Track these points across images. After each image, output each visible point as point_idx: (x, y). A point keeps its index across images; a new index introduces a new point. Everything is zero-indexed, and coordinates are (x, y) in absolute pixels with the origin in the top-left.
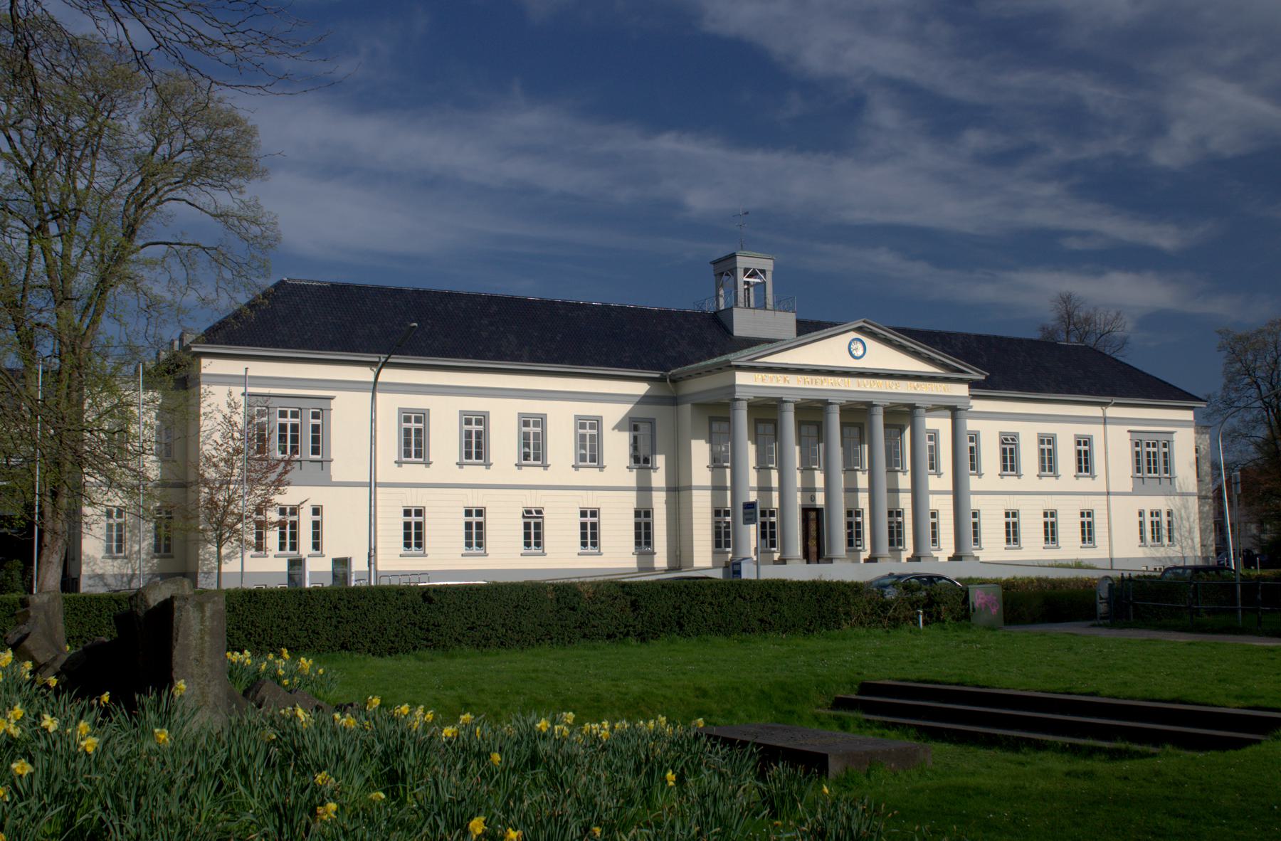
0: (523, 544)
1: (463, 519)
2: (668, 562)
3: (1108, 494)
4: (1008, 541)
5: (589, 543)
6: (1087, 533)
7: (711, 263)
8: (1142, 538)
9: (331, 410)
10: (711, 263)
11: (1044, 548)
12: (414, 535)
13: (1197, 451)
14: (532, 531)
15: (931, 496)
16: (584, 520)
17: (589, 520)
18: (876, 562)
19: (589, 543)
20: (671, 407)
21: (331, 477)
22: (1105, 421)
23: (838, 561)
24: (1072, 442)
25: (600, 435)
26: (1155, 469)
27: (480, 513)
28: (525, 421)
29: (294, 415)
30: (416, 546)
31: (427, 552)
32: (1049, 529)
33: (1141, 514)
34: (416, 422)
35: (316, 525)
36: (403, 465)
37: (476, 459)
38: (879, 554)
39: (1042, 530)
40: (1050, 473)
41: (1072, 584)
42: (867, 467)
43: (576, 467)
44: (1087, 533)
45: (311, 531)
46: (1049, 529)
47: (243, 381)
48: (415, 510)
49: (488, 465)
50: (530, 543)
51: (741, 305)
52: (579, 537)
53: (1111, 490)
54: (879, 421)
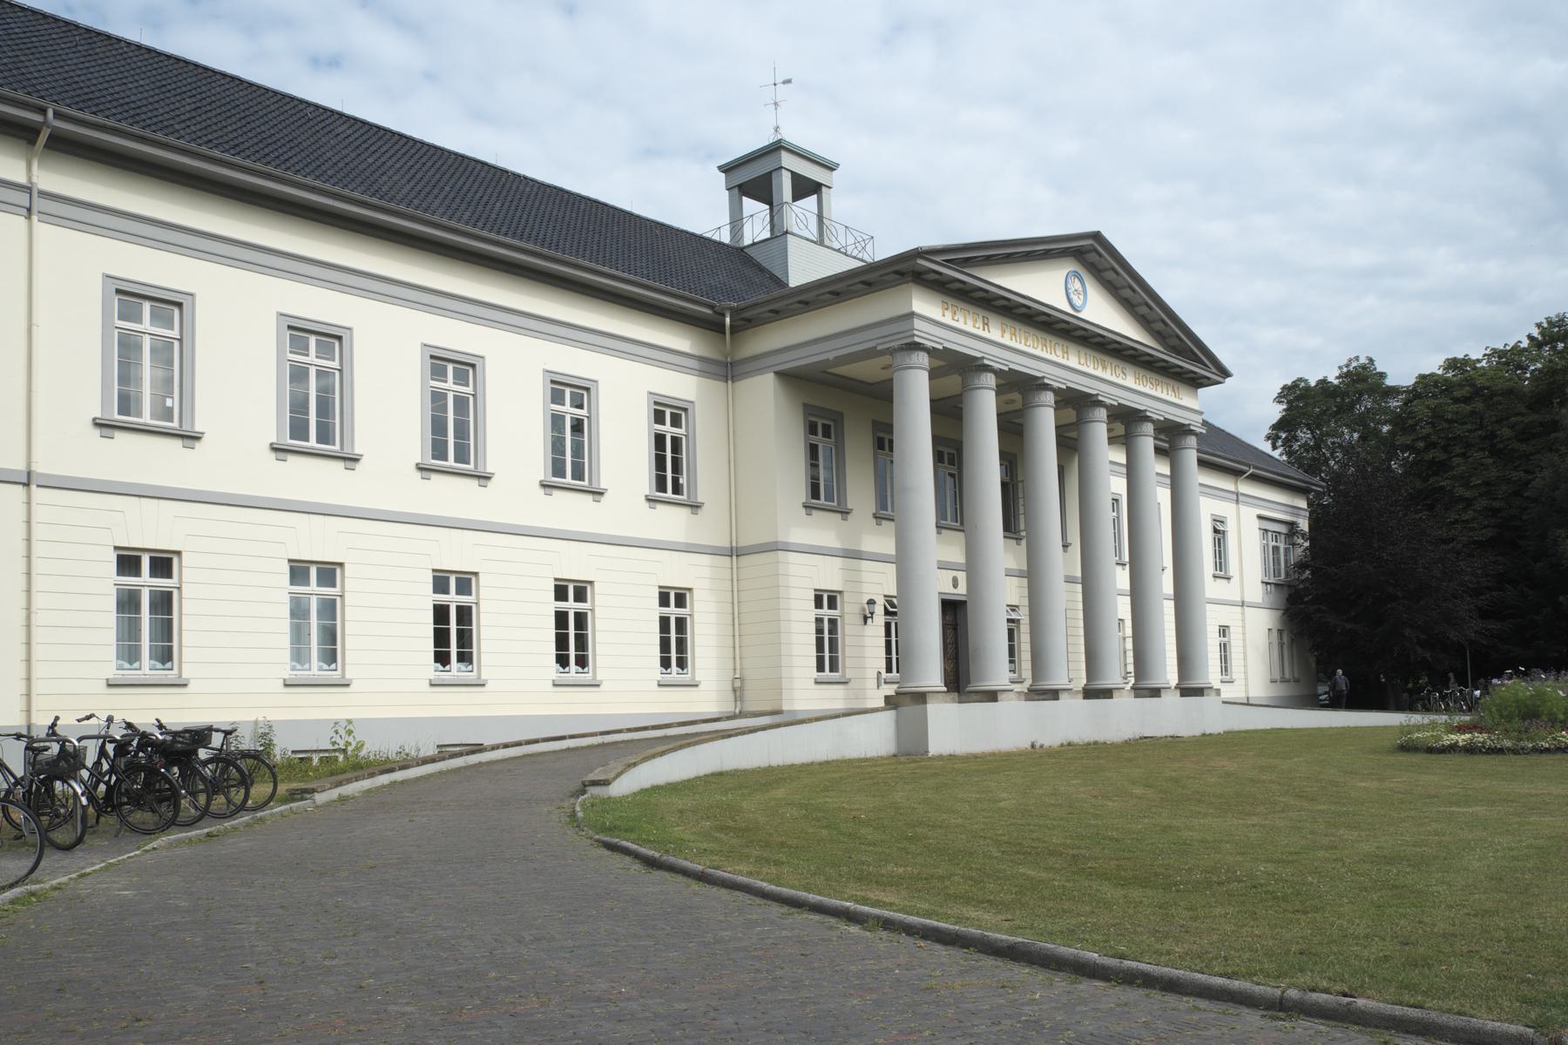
0: (554, 658)
3: (1243, 604)
11: (817, 682)
13: (892, 462)
15: (1208, 606)
18: (1111, 697)
20: (721, 385)
22: (1237, 498)
24: (537, 393)
30: (577, 664)
31: (1234, 677)
32: (673, 635)
39: (285, 625)
42: (1127, 559)
45: (431, 627)
46: (673, 635)
47: (1234, 497)
50: (567, 656)
53: (39, 467)
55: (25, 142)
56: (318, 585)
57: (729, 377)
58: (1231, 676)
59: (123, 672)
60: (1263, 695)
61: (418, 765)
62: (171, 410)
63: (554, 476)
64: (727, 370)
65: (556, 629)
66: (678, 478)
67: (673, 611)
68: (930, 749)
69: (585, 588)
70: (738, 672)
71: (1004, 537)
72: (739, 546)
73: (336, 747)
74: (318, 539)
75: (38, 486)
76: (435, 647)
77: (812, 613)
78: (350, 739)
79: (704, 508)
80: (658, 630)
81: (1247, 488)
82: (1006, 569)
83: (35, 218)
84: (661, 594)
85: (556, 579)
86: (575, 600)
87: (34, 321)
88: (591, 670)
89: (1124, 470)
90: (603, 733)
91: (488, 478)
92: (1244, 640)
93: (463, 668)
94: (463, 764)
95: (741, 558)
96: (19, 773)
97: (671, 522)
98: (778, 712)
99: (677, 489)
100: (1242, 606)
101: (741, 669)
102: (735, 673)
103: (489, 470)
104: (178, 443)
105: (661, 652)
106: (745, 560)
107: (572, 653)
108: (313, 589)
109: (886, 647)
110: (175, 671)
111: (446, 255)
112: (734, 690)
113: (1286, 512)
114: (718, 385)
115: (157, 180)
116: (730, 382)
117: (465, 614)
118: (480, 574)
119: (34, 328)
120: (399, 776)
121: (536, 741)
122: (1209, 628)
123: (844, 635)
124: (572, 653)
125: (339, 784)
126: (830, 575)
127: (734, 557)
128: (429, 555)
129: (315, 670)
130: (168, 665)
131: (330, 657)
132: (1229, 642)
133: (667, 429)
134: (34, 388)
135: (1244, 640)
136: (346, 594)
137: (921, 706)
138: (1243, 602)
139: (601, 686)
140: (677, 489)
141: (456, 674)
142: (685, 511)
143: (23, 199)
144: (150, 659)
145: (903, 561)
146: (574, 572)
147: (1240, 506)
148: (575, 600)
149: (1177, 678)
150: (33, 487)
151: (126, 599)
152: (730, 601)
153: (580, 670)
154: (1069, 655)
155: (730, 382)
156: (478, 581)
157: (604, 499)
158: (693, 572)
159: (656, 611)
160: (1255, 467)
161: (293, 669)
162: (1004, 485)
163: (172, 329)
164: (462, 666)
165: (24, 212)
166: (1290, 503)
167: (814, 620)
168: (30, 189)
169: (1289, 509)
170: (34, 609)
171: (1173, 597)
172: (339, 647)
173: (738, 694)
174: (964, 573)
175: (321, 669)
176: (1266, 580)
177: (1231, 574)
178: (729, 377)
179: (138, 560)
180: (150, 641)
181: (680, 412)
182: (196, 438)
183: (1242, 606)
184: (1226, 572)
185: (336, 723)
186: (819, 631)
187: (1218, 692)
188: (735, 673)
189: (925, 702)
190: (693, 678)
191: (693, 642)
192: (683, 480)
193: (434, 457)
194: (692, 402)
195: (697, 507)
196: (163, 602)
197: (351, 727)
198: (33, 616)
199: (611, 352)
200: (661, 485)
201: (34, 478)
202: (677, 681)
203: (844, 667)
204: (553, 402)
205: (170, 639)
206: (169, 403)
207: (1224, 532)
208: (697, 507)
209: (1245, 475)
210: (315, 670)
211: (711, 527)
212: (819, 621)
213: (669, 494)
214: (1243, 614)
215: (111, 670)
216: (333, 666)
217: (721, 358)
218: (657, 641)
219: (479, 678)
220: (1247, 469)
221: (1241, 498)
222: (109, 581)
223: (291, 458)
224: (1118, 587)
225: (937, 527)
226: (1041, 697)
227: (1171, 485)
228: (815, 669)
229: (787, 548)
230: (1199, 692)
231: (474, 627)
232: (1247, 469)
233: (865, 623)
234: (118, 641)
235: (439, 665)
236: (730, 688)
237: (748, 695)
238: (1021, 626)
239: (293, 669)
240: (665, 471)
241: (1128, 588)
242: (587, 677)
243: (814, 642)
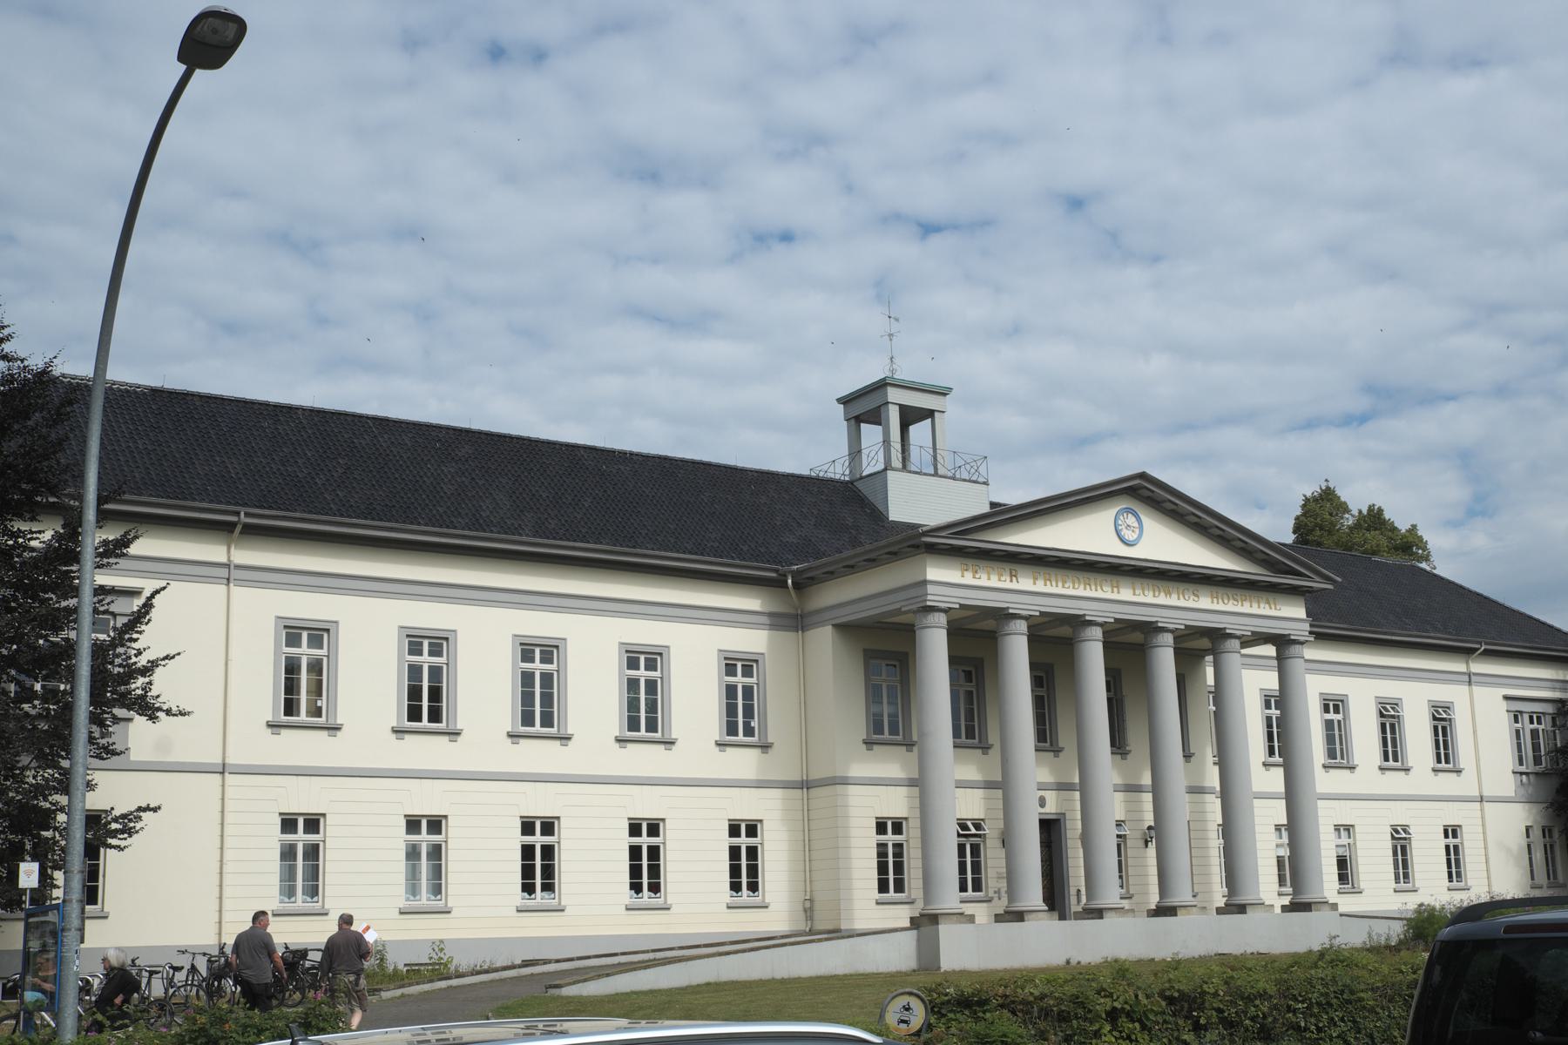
1: (517, 840)
3: (1482, 799)
4: (883, 887)
7: (839, 400)
10: (839, 400)
15: (1320, 803)
17: (743, 841)
18: (1176, 915)
22: (1470, 679)
23: (1034, 915)
26: (1447, 756)
27: (313, 824)
28: (414, 642)
30: (650, 890)
31: (1469, 884)
34: (431, 654)
37: (430, 721)
38: (1182, 895)
40: (970, 741)
41: (1127, 963)
43: (621, 741)
47: (1467, 678)
51: (896, 462)
52: (1336, 867)
55: (226, 532)
56: (428, 833)
57: (800, 627)
58: (1466, 882)
59: (431, 902)
60: (787, 929)
61: (472, 975)
62: (320, 709)
63: (728, 735)
64: (793, 621)
65: (630, 861)
66: (750, 722)
67: (1451, 841)
68: (942, 965)
69: (658, 825)
70: (808, 894)
71: (1112, 753)
72: (809, 778)
73: (433, 961)
74: (426, 800)
75: (230, 773)
76: (523, 879)
77: (873, 839)
78: (442, 956)
79: (344, 728)
80: (520, 859)
81: (1479, 667)
82: (1038, 783)
83: (231, 585)
84: (731, 826)
85: (629, 819)
86: (747, 836)
87: (229, 658)
88: (662, 896)
89: (1275, 663)
90: (654, 951)
91: (569, 739)
92: (1485, 840)
93: (547, 897)
94: (516, 975)
95: (811, 790)
96: (205, 975)
97: (744, 762)
98: (838, 931)
99: (749, 731)
100: (1481, 801)
101: (811, 891)
102: (806, 895)
103: (569, 732)
104: (325, 733)
105: (731, 878)
106: (814, 792)
107: (744, 880)
108: (301, 837)
109: (1394, 864)
110: (320, 903)
111: (496, 557)
112: (805, 910)
113: (1554, 689)
114: (789, 636)
115: (424, 553)
116: (800, 632)
117: (654, 852)
118: (449, 817)
119: (229, 662)
120: (454, 982)
121: (588, 957)
122: (1322, 829)
123: (909, 858)
124: (744, 880)
125: (403, 986)
126: (896, 803)
127: (805, 790)
128: (517, 805)
129: (424, 901)
130: (315, 899)
131: (437, 890)
132: (1462, 843)
133: (739, 680)
134: (228, 704)
135: (1485, 840)
136: (449, 840)
137: (934, 927)
138: (1482, 797)
139: (566, 911)
140: (749, 731)
141: (301, 904)
142: (755, 752)
143: (224, 572)
144: (303, 894)
145: (919, 783)
146: (646, 812)
147: (1474, 688)
148: (747, 836)
149: (1158, 896)
150: (227, 775)
151: (287, 849)
152: (802, 829)
153: (751, 894)
154: (1194, 867)
155: (800, 632)
156: (664, 826)
157: (1411, 772)
158: (766, 807)
159: (726, 841)
160: (1486, 644)
161: (408, 900)
162: (1109, 700)
163: (322, 648)
164: (545, 894)
165: (225, 581)
166: (1561, 678)
167: (875, 846)
168: (229, 565)
169: (1558, 685)
170: (224, 861)
171: (1284, 796)
172: (443, 882)
173: (808, 914)
174: (1151, 794)
175: (428, 899)
176: (1523, 769)
177: (1356, 763)
178: (800, 627)
179: (296, 821)
180: (303, 881)
181: (655, 657)
182: (337, 728)
183: (1481, 801)
184: (1348, 762)
185: (433, 943)
186: (1448, 853)
187: (1334, 906)
188: (806, 895)
189: (937, 923)
190: (1414, 886)
191: (986, 863)
192: (755, 723)
193: (629, 730)
194: (762, 654)
195: (767, 747)
196: (313, 852)
197: (442, 946)
198: (224, 866)
199: (306, 588)
200: (732, 729)
201: (227, 769)
202: (301, 910)
203: (910, 888)
204: (727, 675)
205: (440, 879)
206: (319, 703)
207: (1450, 719)
208: (767, 747)
209: (1479, 652)
210: (424, 901)
211: (784, 764)
212: (1447, 847)
213: (643, 733)
214: (1482, 810)
215: (402, 903)
216: (439, 897)
217: (792, 611)
218: (875, 865)
219: (665, 902)
220: (1479, 646)
221: (1473, 678)
222: (274, 837)
223: (284, 732)
224: (1318, 791)
225: (1184, 756)
226: (1090, 916)
227: (1278, 667)
228: (877, 891)
229: (845, 781)
230: (1242, 909)
231: (556, 862)
232: (1479, 646)
233: (1147, 846)
234: (281, 881)
235: (526, 894)
236: (801, 908)
237: (818, 915)
238: (987, 840)
239: (408, 900)
240: (1273, 742)
241: (1283, 790)
242: (757, 900)
243: (876, 866)
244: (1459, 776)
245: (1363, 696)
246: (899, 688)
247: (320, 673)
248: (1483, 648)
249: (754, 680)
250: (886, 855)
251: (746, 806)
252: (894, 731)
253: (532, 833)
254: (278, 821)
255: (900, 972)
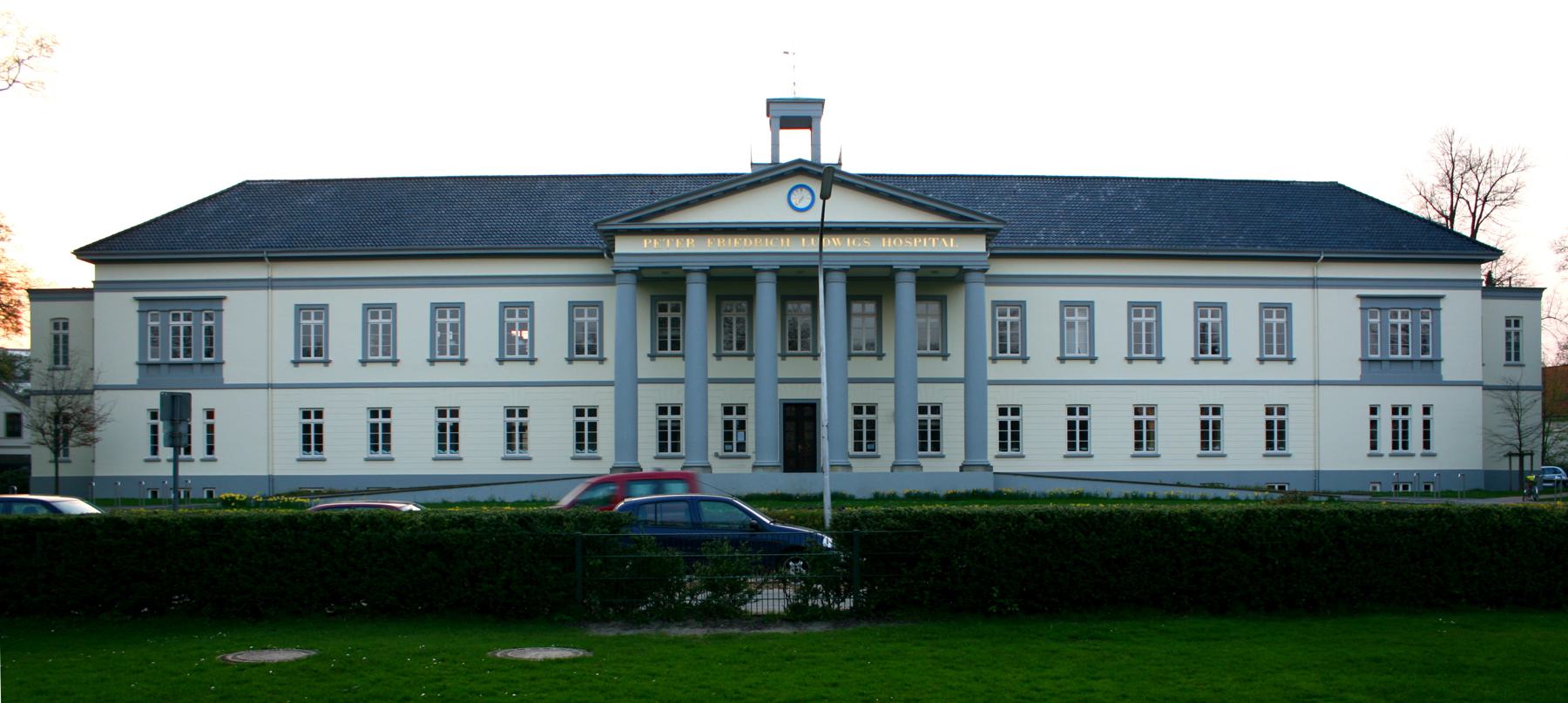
0: (1200, 444)
1: (1263, 418)
2: (64, 477)
5: (313, 448)
6: (1275, 435)
8: (1374, 446)
9: (1440, 309)
12: (313, 438)
14: (1078, 431)
16: (1003, 418)
17: (1078, 418)
19: (313, 448)
21: (1441, 377)
25: (1289, 322)
29: (188, 318)
30: (315, 450)
33: (1373, 410)
35: (1427, 424)
36: (657, 358)
44: (1275, 435)
45: (150, 435)
48: (1278, 409)
49: (327, 363)
52: (324, 437)
54: (766, 293)
76: (1000, 440)
148: (1080, 415)
149: (894, 457)
160: (1325, 252)
244: (396, 365)
245: (1111, 305)
246: (746, 322)
247: (212, 334)
248: (1322, 257)
249: (1378, 320)
250: (926, 427)
251: (586, 398)
252: (1280, 351)
253: (309, 417)
254: (1199, 409)
255: (1044, 494)
